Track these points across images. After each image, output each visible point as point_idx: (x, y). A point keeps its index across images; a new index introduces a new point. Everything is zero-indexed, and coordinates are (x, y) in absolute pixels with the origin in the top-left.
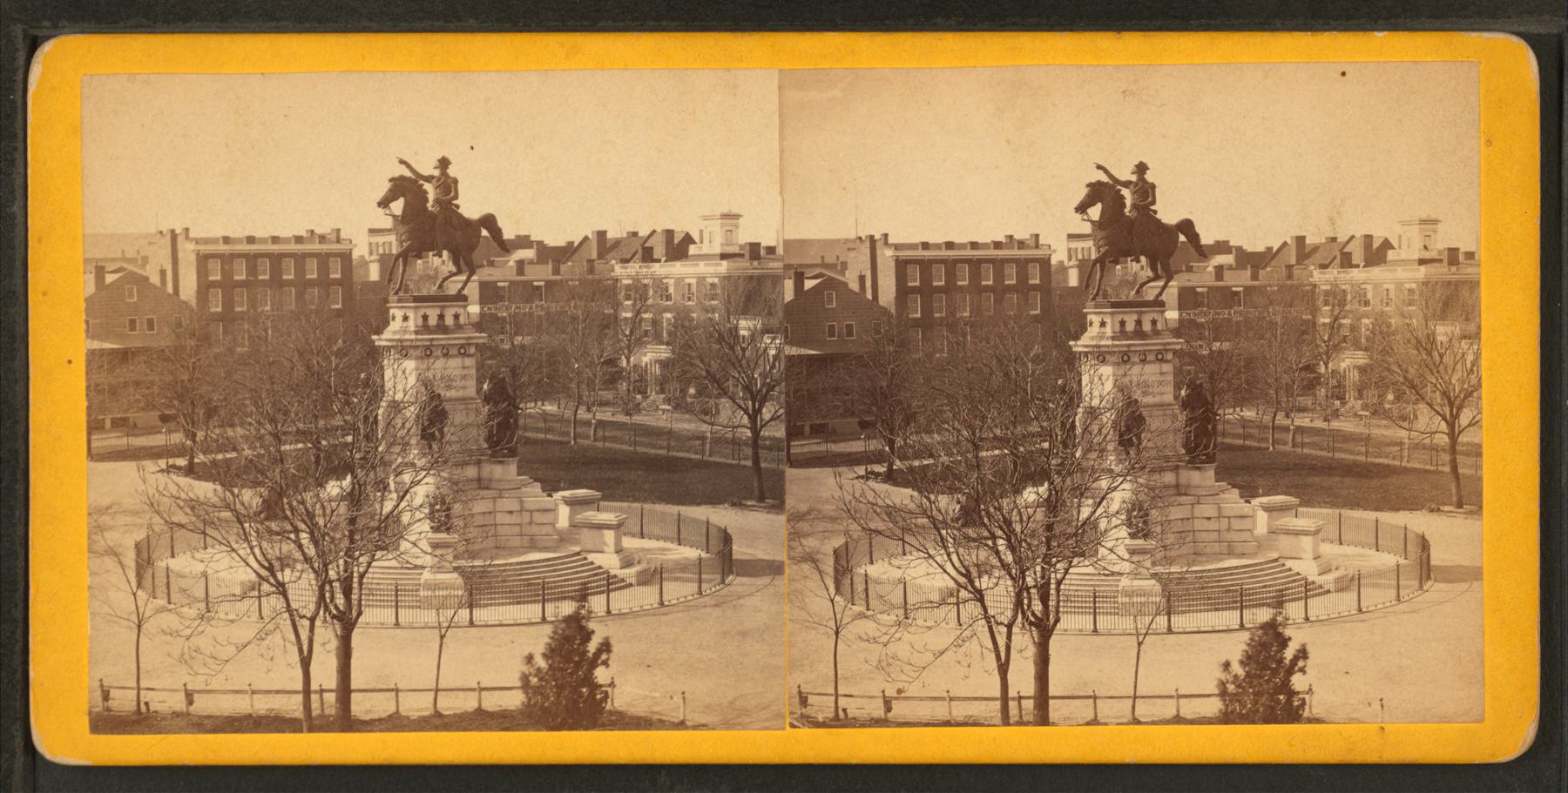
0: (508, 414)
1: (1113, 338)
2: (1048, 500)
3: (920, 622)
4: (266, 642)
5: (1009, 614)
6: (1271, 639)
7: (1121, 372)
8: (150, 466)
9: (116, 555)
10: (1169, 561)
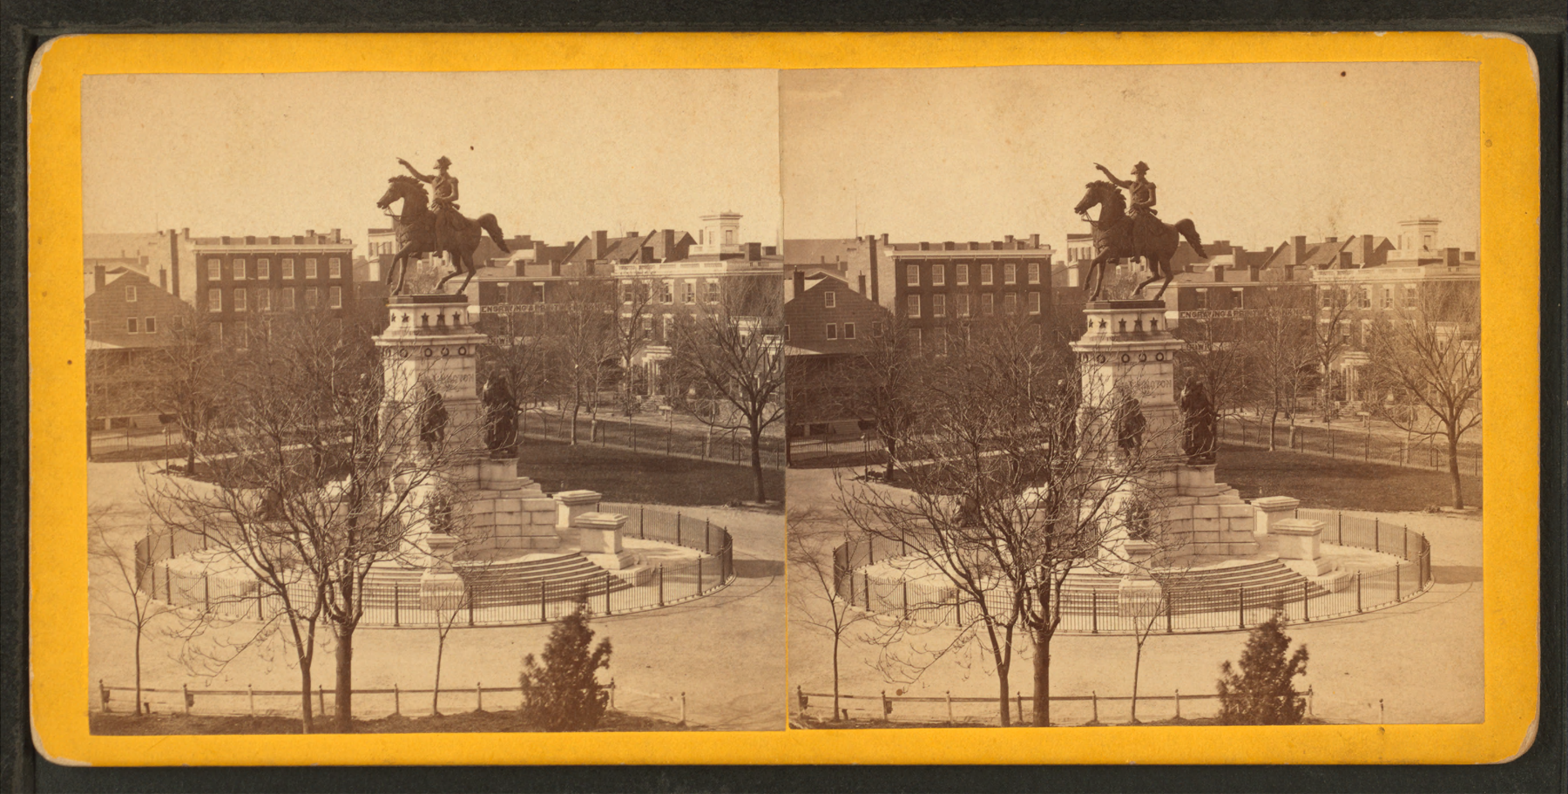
1: (1113, 339)
2: (1048, 501)
3: (920, 623)
4: (266, 643)
5: (1009, 614)
6: (1271, 640)
7: (1121, 372)
8: (150, 466)
9: (116, 556)
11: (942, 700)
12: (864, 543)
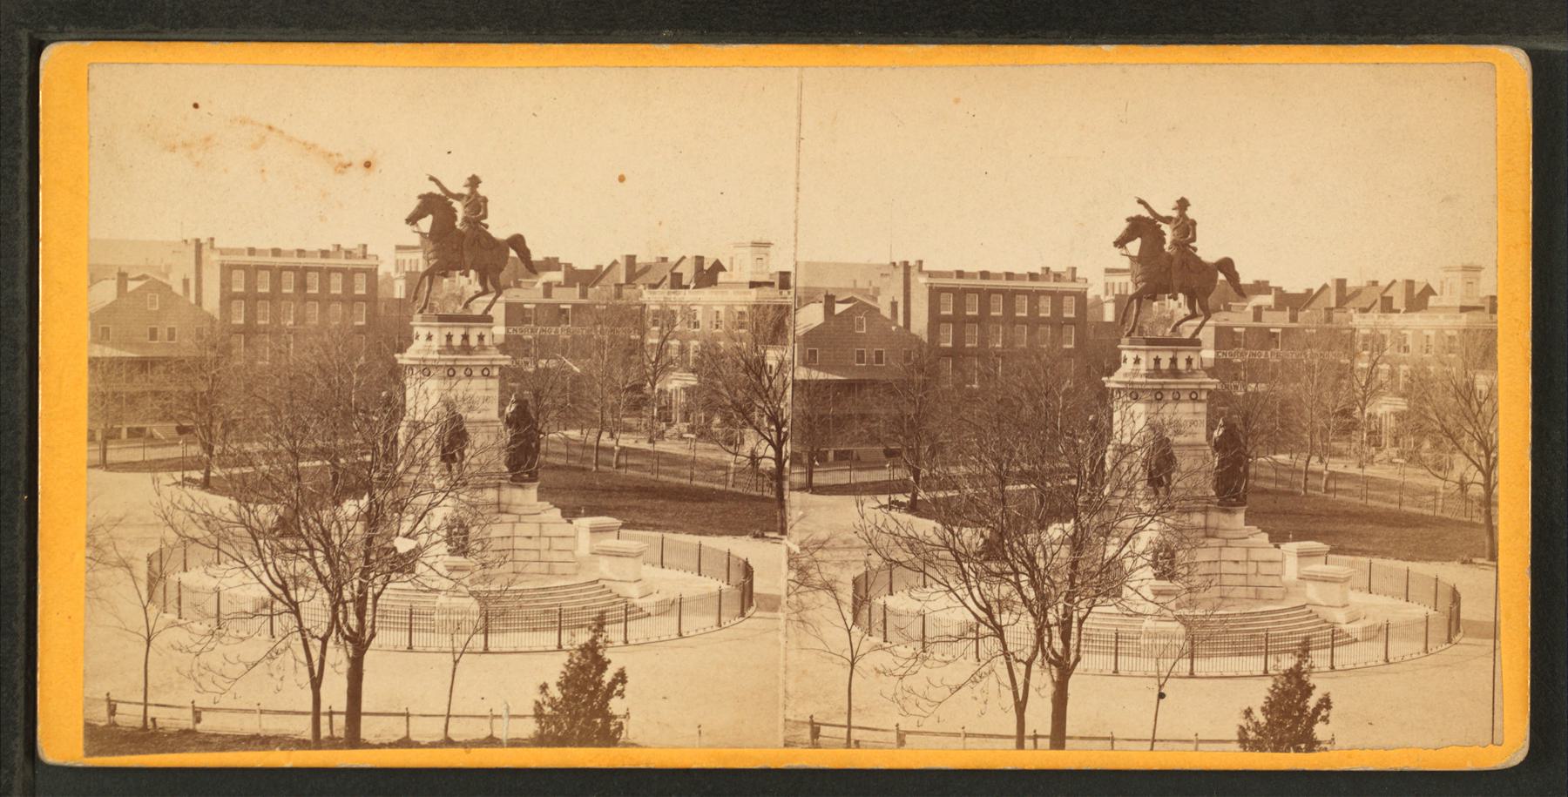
0: (1239, 462)
2: (1073, 537)
3: (938, 656)
5: (1029, 651)
6: (593, 658)
7: (1153, 410)
8: (165, 478)
9: (128, 567)
10: (1192, 604)
11: (958, 735)
12: (179, 553)
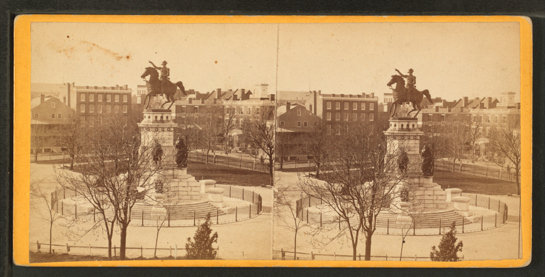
1: (399, 131)
2: (373, 187)
3: (326, 228)
4: (96, 230)
5: (358, 226)
6: (206, 229)
7: (401, 142)
8: (57, 166)
10: (414, 210)
11: (333, 255)
12: (62, 192)
